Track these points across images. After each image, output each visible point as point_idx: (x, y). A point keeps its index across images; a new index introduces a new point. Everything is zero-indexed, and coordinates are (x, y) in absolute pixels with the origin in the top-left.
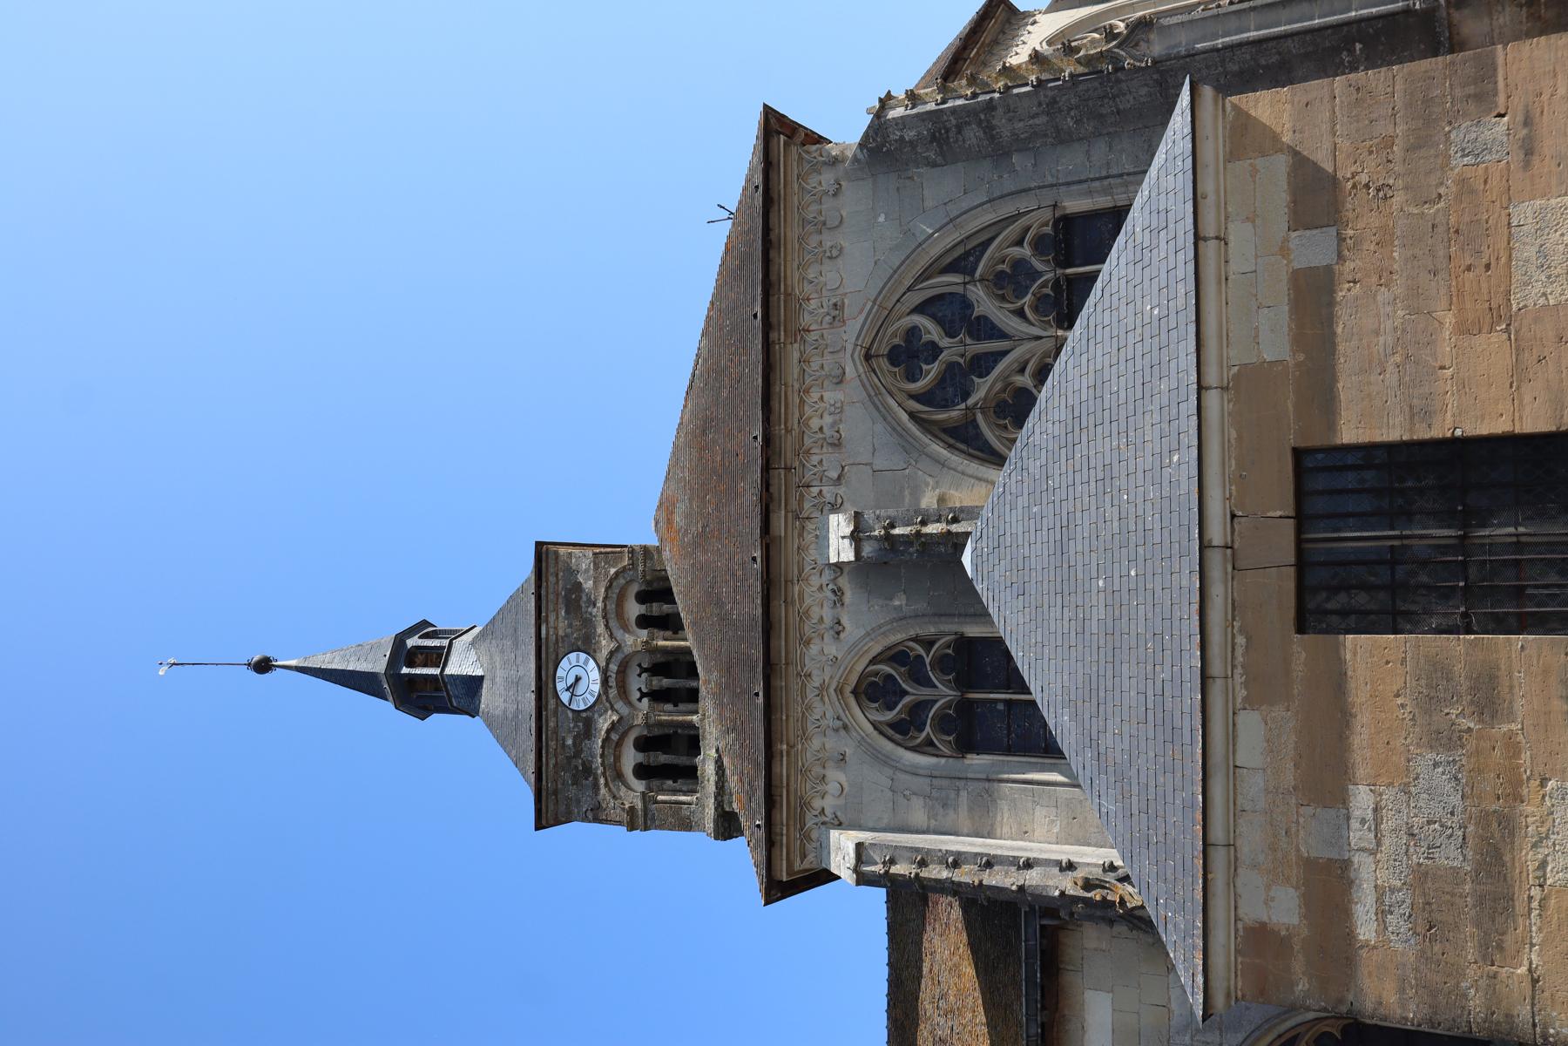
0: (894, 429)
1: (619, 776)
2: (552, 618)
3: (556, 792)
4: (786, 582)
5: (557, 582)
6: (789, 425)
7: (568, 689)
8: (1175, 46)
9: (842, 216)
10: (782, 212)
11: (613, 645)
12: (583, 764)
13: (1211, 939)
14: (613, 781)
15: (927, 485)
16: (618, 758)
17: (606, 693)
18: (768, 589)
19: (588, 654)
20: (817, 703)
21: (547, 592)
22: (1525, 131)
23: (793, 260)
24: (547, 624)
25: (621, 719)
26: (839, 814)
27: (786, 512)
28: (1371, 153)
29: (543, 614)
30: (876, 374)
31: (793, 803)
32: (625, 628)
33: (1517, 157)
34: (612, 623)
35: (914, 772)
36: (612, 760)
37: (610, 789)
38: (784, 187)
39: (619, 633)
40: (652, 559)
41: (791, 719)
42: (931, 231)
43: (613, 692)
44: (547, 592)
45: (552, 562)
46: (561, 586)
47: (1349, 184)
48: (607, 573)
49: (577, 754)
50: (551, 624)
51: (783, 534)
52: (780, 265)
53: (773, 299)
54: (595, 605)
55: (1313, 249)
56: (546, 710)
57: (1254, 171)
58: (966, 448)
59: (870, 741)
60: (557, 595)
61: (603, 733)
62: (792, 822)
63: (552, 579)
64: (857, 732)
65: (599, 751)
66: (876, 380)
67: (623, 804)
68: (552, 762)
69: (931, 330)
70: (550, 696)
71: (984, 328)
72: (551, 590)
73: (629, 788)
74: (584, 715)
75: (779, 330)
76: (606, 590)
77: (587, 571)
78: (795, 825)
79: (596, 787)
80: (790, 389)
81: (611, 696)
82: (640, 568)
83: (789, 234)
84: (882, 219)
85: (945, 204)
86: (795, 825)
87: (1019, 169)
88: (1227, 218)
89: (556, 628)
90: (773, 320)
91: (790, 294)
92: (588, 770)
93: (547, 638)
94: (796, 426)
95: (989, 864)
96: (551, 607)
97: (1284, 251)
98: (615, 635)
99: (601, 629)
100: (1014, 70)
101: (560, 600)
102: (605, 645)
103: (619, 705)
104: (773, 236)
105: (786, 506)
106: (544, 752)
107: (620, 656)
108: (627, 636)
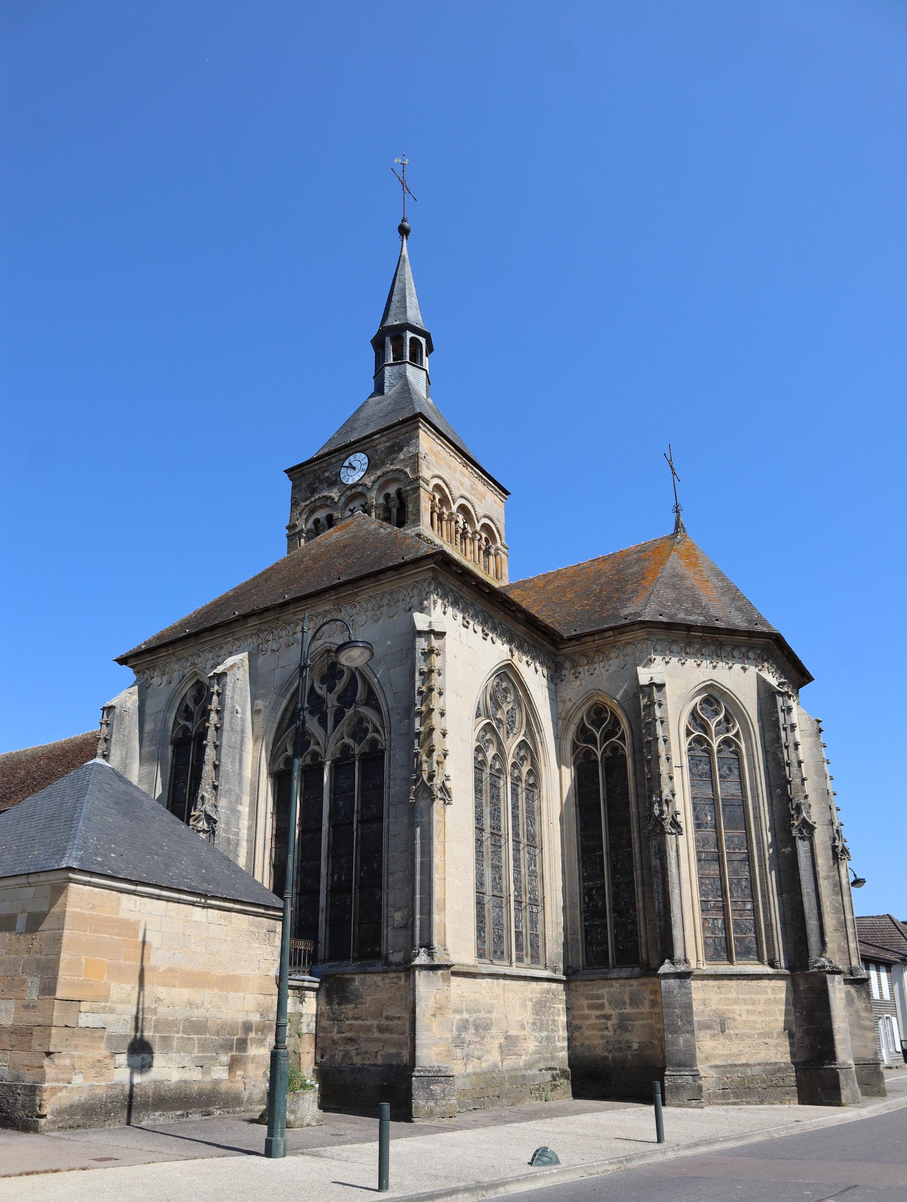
0: (291, 676)
1: (312, 512)
2: (384, 439)
3: (303, 475)
4: (232, 633)
5: (404, 434)
6: (297, 614)
7: (350, 464)
8: (421, 814)
9: (393, 616)
10: (393, 578)
11: (369, 484)
12: (316, 487)
13: (10, 879)
14: (309, 509)
15: (266, 702)
16: (321, 507)
17: (348, 489)
18: (222, 626)
19: (367, 470)
20: (189, 664)
21: (396, 430)
22: (31, 1006)
23: (373, 592)
24: (380, 437)
25: (336, 503)
26: (151, 686)
27: (260, 624)
28: (40, 945)
29: (385, 433)
30: (320, 658)
31: (153, 661)
32: (380, 489)
33: (25, 1002)
34: (381, 480)
35: (165, 721)
36: (318, 505)
37: (304, 509)
38: (408, 575)
39: (376, 486)
40: (414, 493)
41: (183, 651)
42: (378, 676)
43: (349, 493)
44: (396, 430)
45: (413, 427)
46: (401, 437)
47: (34, 937)
48: (406, 466)
49: (321, 482)
50: (381, 440)
51: (248, 625)
52: (368, 585)
53: (350, 587)
54: (391, 464)
55: (21, 923)
56: (339, 454)
57: (46, 897)
58: (288, 717)
59: (177, 695)
60: (397, 437)
61: (330, 494)
62: (147, 663)
63: (404, 430)
64: (179, 688)
65: (321, 495)
66: (317, 659)
67: (298, 519)
68: (316, 468)
69: (341, 685)
70: (346, 453)
71: (339, 715)
72: (398, 432)
73: (307, 520)
74: (339, 479)
75: (336, 595)
76: (397, 469)
77: (409, 452)
78: (148, 665)
79: (305, 500)
80: (313, 609)
81: (347, 492)
82: (408, 488)
83: (386, 585)
84: (389, 643)
85: (390, 682)
86: (148, 665)
87: (401, 725)
88: (37, 886)
89: (380, 443)
90: (340, 590)
91: (357, 595)
92: (313, 491)
93: (373, 440)
94: (297, 617)
95: (216, 747)
96: (390, 436)
97: (23, 911)
98: (376, 484)
99: (379, 473)
100: (429, 716)
101: (394, 440)
102: (368, 481)
103: (343, 499)
104: (381, 576)
105: (262, 623)
106: (320, 461)
107: (365, 491)
108: (375, 491)
